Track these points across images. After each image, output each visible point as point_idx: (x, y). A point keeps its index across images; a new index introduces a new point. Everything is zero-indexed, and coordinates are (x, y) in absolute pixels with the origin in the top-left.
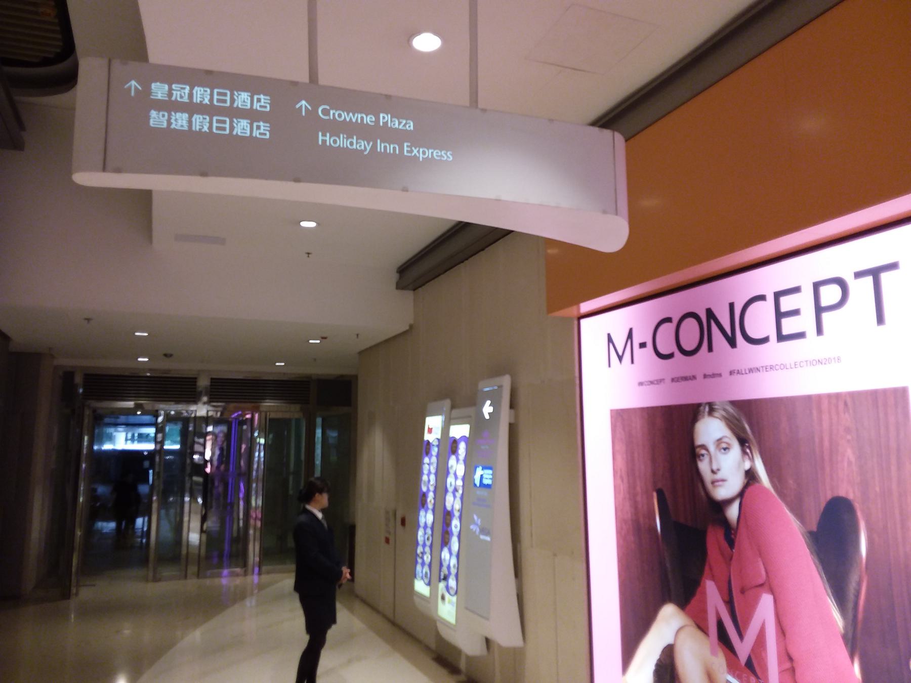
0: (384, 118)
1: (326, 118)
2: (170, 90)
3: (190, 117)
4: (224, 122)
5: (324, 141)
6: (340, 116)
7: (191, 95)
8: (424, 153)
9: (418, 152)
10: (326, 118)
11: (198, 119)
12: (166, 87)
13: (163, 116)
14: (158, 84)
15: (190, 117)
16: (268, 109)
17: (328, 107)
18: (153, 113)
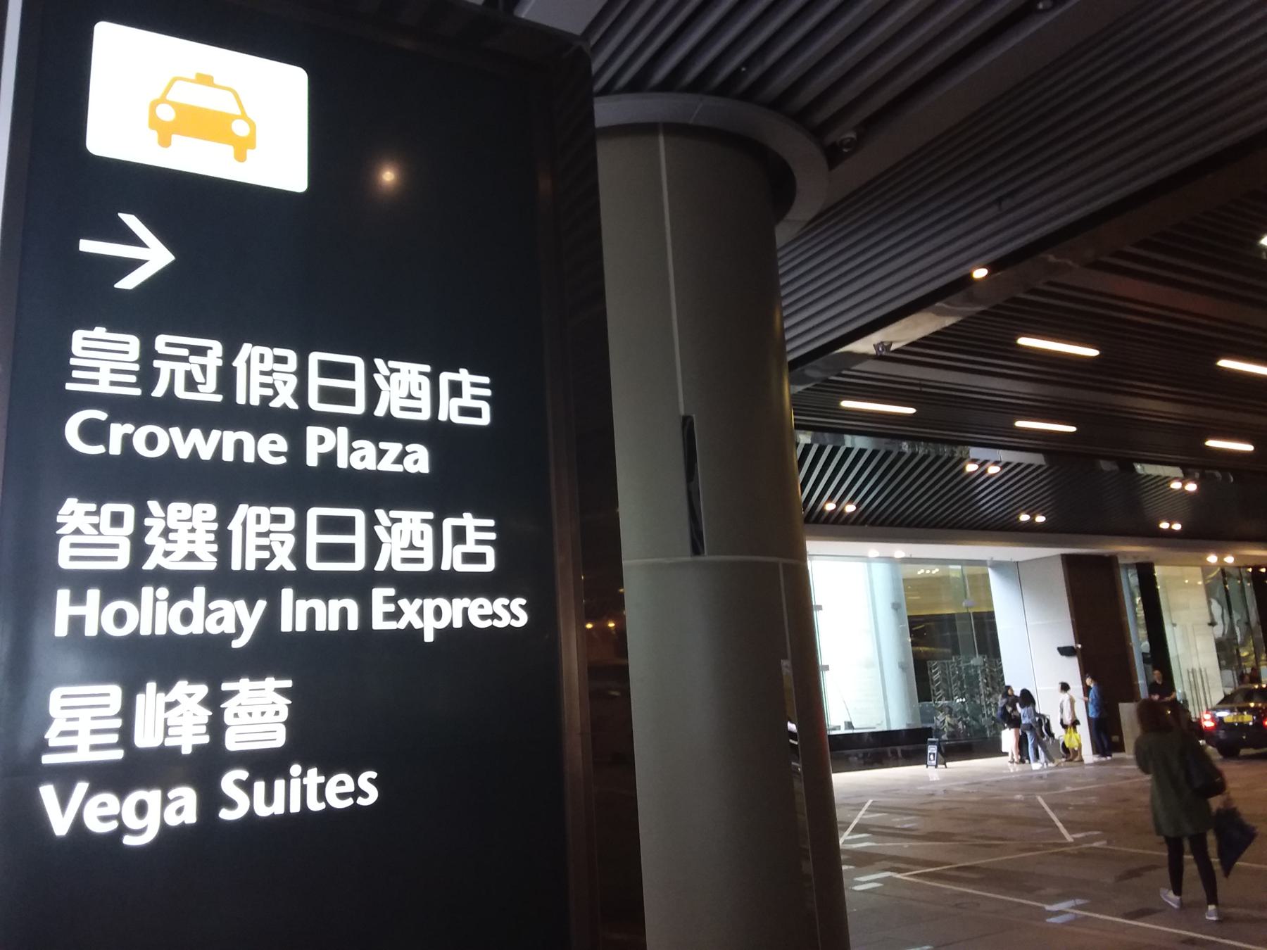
0: (321, 440)
1: (99, 450)
2: (149, 353)
3: (225, 516)
4: (346, 526)
5: (77, 623)
6: (152, 441)
7: (226, 378)
8: (438, 613)
9: (420, 612)
10: (99, 450)
11: (250, 518)
12: (133, 344)
13: (117, 519)
14: (100, 332)
15: (225, 516)
16: (485, 420)
17: (101, 415)
18: (74, 514)
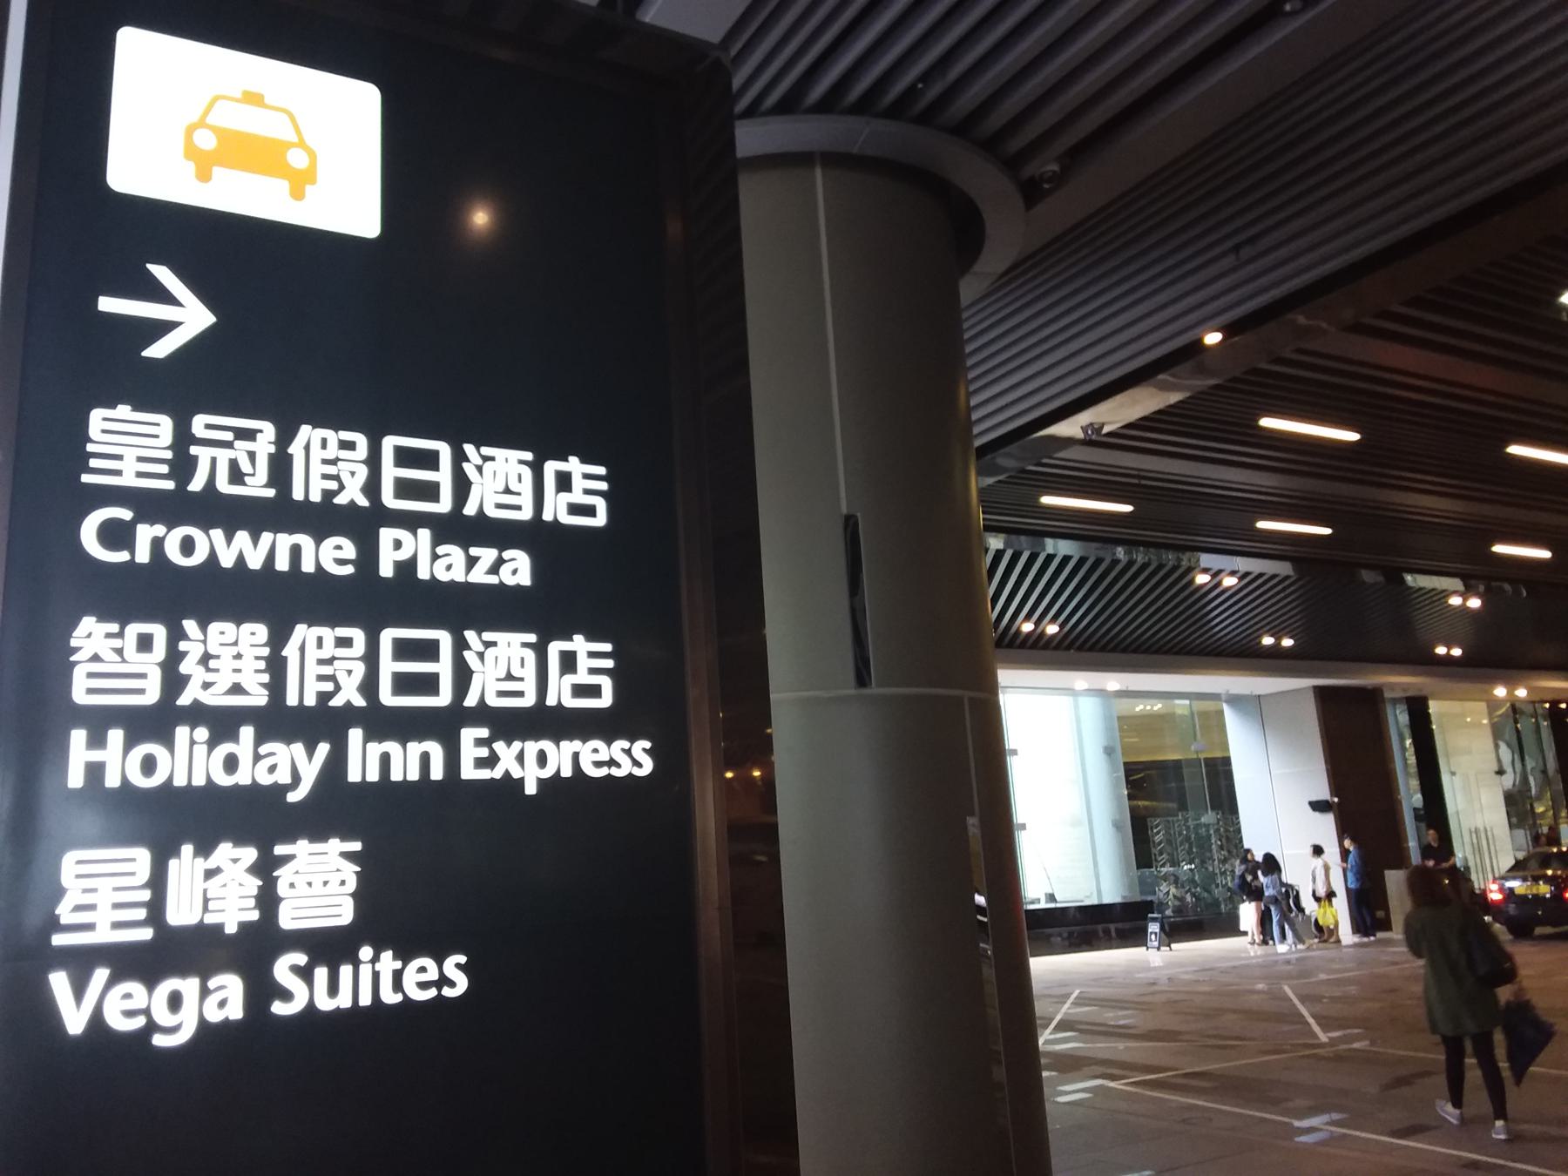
0: (398, 545)
1: (122, 556)
2: (184, 437)
3: (278, 639)
4: (428, 651)
5: (95, 771)
6: (188, 546)
7: (280, 468)
8: (542, 759)
9: (520, 758)
10: (122, 556)
11: (310, 642)
12: (164, 426)
13: (145, 643)
14: (124, 411)
15: (278, 639)
16: (600, 520)
17: (126, 514)
18: (91, 636)
